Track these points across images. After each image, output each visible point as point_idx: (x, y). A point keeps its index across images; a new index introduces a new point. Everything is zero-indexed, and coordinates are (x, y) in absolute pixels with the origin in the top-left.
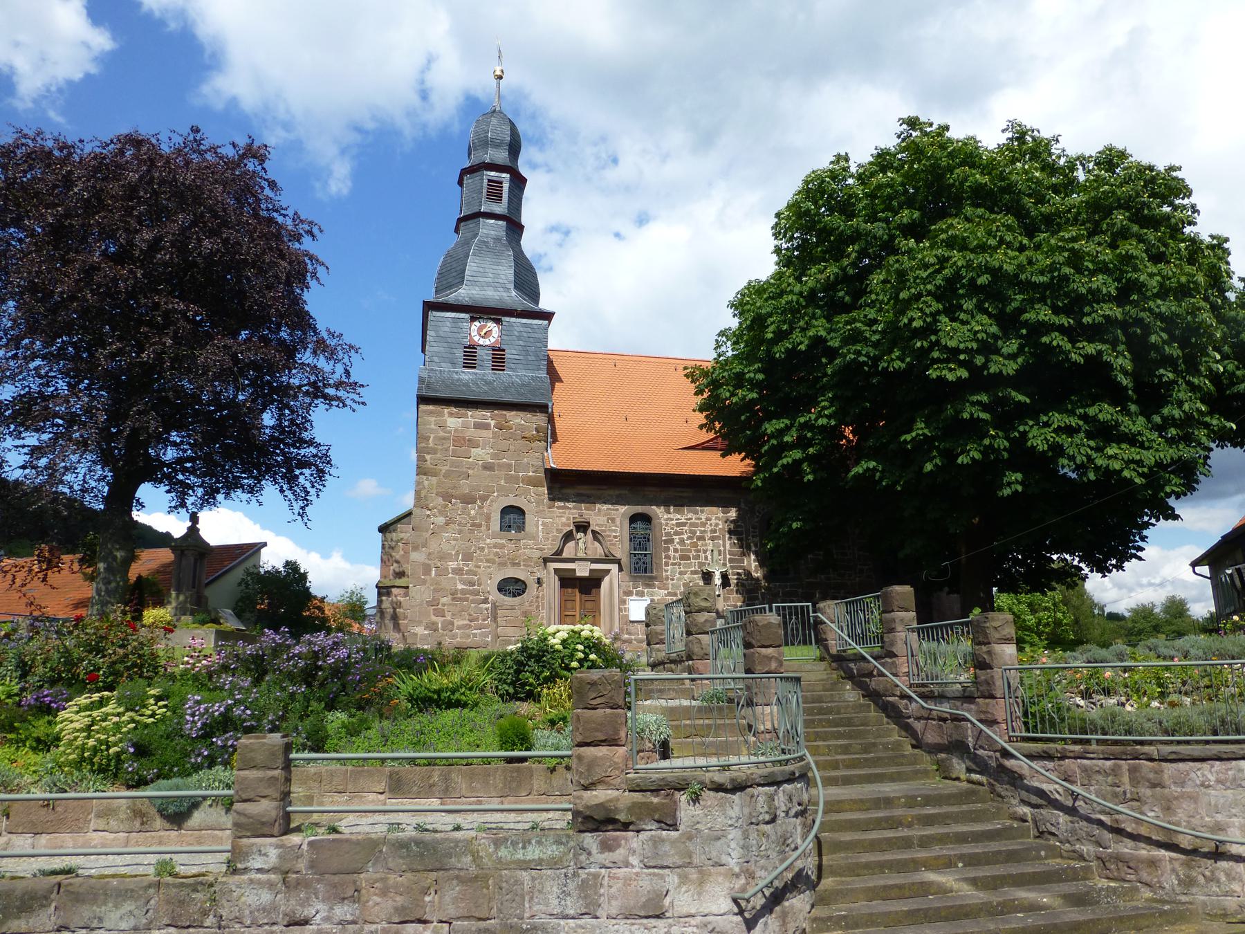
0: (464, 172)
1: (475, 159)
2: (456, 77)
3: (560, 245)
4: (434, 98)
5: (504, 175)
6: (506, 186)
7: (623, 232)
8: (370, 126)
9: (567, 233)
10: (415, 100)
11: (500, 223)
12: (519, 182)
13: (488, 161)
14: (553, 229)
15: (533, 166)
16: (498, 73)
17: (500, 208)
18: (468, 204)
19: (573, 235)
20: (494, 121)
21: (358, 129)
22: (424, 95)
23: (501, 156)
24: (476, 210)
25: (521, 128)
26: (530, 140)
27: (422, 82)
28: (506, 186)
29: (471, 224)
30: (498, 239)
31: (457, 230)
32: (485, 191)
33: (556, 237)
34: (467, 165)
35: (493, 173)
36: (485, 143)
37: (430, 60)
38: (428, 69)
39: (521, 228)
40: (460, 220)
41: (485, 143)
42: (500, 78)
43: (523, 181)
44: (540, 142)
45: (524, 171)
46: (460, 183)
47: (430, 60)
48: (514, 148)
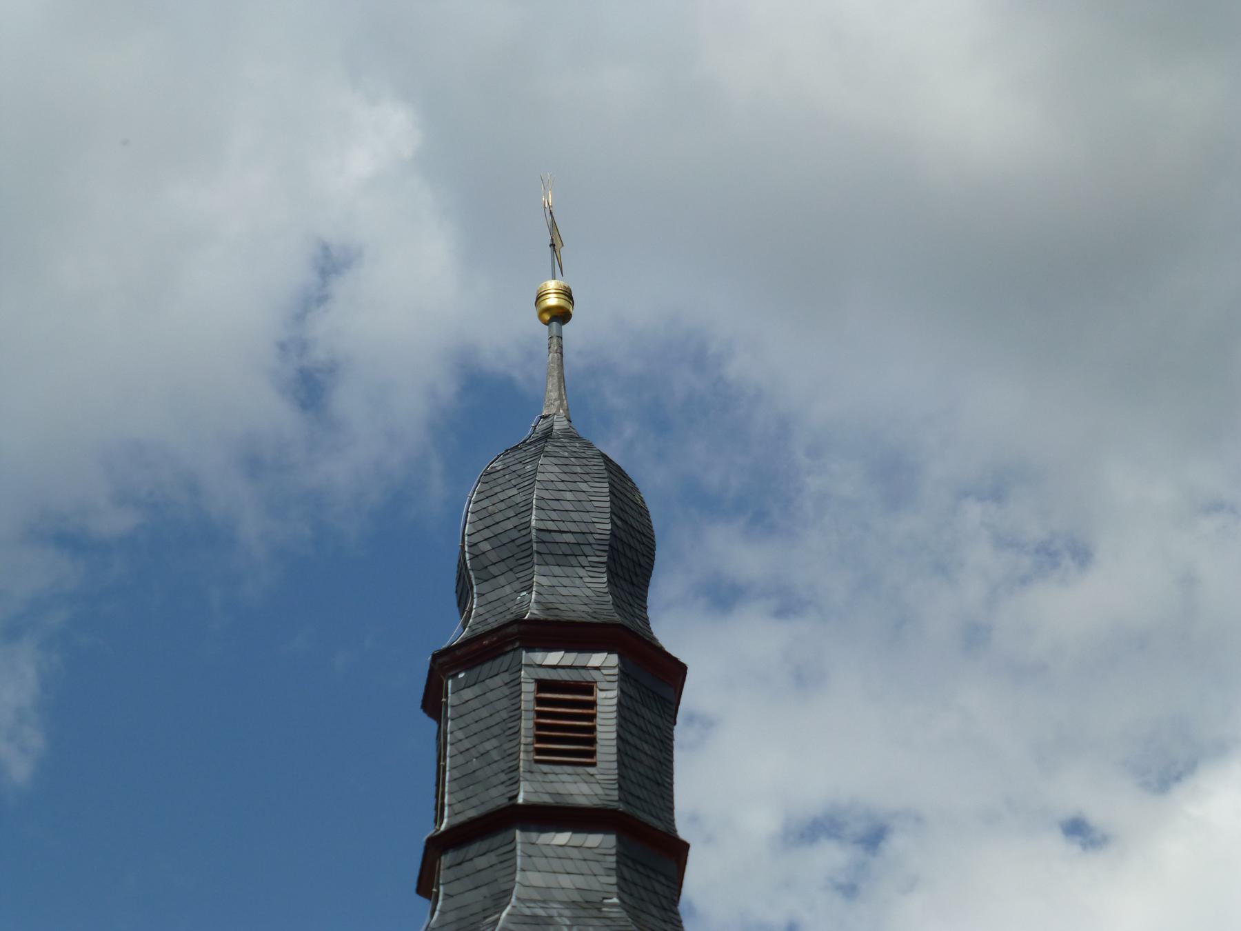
0: (447, 663)
1: (486, 611)
2: (429, 302)
3: (849, 890)
4: (346, 400)
5: (597, 659)
6: (607, 699)
7: (1096, 814)
8: (116, 522)
9: (874, 838)
10: (273, 413)
11: (594, 840)
12: (657, 681)
13: (533, 612)
14: (815, 829)
15: (723, 596)
16: (552, 301)
17: (584, 787)
18: (467, 779)
19: (897, 843)
20: (548, 469)
21: (69, 540)
22: (310, 387)
23: (582, 591)
24: (495, 798)
25: (653, 483)
26: (705, 503)
27: (304, 346)
28: (607, 699)
29: (480, 857)
30: (586, 906)
31: (426, 885)
32: (527, 724)
33: (831, 857)
34: (456, 634)
35: (554, 658)
36: (520, 551)
37: (331, 264)
38: (323, 299)
39: (678, 851)
40: (437, 846)
41: (520, 551)
42: (561, 316)
43: (672, 673)
44: (763, 504)
45: (670, 630)
46: (433, 703)
47: (331, 264)
48: (630, 554)
